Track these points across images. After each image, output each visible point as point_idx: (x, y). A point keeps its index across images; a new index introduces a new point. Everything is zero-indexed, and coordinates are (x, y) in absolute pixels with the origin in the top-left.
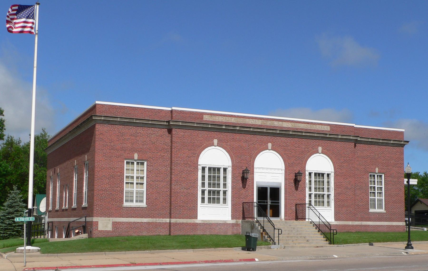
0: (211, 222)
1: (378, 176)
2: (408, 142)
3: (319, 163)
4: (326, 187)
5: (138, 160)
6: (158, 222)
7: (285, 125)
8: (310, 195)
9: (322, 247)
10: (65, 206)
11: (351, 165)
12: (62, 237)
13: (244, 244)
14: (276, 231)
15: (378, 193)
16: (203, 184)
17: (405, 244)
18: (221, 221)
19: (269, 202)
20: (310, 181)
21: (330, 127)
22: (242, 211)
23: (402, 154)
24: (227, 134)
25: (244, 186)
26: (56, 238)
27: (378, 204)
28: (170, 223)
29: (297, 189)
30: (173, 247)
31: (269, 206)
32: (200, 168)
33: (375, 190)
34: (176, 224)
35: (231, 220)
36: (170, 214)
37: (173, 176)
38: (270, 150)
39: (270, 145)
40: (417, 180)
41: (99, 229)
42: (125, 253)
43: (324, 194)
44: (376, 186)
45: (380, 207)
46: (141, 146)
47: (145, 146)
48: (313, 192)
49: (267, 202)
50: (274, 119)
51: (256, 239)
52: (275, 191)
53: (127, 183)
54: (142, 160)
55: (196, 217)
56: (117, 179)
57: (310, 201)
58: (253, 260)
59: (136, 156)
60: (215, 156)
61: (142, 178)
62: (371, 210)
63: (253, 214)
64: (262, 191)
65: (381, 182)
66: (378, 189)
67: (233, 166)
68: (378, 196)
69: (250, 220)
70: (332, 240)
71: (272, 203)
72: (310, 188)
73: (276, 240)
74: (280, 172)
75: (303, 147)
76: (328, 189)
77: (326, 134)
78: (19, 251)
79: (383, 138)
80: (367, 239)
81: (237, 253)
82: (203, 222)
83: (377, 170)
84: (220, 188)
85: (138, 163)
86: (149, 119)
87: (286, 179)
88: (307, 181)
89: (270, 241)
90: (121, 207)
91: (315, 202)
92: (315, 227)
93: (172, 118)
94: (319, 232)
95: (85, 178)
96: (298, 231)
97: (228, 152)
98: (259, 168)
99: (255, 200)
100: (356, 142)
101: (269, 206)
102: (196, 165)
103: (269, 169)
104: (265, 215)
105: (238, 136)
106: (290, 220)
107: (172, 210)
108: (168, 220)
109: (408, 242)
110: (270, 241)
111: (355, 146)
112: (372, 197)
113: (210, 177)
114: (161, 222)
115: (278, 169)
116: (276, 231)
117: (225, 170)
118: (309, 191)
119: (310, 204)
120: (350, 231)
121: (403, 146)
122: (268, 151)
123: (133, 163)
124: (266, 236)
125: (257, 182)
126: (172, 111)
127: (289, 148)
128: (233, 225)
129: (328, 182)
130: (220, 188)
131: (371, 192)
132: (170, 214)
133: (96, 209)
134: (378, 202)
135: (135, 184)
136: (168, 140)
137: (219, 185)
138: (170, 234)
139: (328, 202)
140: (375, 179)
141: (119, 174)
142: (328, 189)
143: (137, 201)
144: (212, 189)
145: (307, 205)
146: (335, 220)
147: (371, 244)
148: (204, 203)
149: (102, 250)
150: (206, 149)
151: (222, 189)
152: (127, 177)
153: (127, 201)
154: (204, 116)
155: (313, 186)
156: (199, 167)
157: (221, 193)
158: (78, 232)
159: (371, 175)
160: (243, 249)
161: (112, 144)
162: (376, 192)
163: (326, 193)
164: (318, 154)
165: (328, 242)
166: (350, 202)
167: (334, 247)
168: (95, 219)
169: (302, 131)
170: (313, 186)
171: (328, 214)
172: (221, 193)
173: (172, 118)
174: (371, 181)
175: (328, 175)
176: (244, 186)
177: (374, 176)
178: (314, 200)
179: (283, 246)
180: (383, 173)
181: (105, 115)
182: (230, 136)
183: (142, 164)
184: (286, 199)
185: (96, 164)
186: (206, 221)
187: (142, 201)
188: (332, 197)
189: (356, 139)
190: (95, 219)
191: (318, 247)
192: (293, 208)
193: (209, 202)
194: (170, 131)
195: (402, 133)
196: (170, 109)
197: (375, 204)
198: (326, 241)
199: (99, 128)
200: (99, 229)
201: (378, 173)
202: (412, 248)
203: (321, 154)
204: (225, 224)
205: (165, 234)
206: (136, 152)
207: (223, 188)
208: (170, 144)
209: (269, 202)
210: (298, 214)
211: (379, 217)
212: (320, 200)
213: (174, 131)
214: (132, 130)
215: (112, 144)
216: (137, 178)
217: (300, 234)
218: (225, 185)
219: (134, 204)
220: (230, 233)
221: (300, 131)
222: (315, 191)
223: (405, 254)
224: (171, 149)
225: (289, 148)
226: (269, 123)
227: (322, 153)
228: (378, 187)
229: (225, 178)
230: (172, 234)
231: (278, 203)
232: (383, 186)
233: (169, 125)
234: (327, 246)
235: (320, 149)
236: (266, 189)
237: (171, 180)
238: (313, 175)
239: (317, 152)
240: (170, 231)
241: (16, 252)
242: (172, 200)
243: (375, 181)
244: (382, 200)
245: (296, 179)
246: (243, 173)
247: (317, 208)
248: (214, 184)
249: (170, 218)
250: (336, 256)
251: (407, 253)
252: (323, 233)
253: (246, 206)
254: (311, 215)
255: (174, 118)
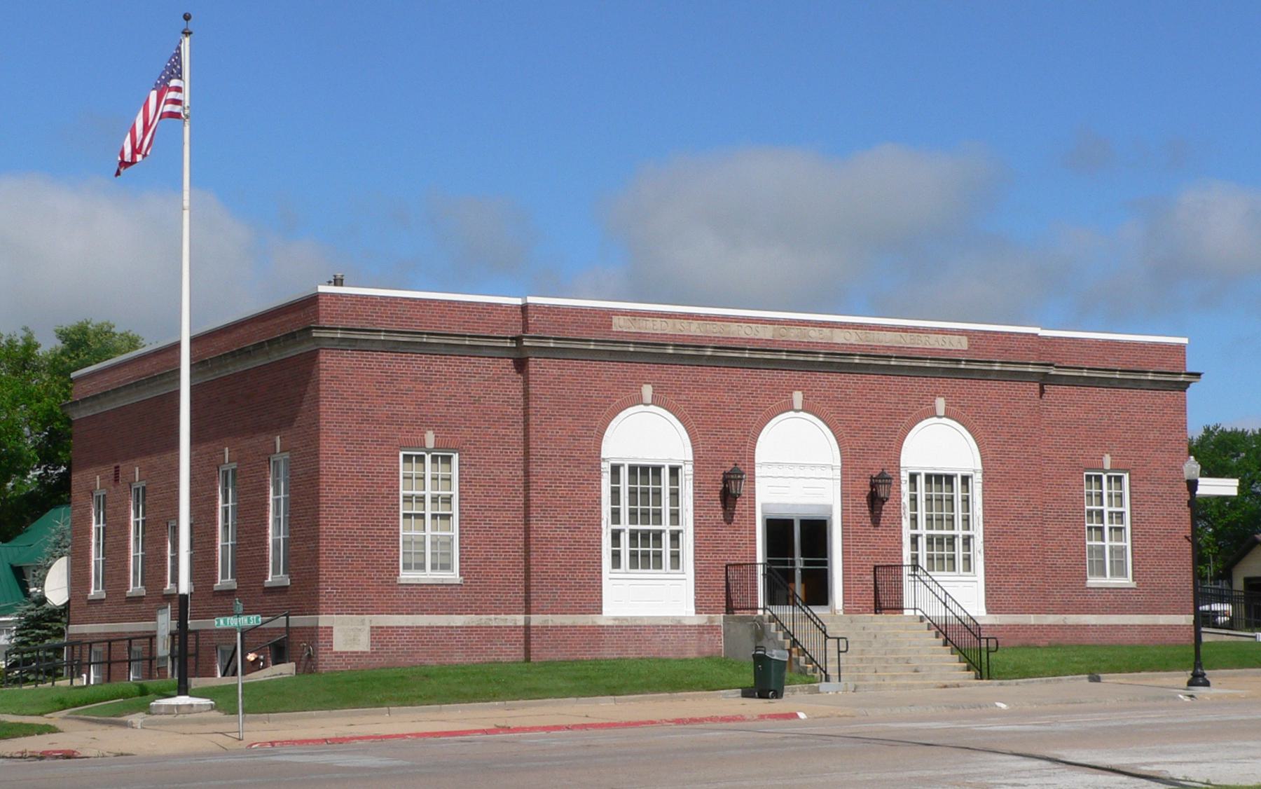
0: (638, 623)
1: (1109, 478)
2: (1198, 375)
3: (939, 445)
4: (959, 514)
5: (436, 448)
6: (494, 624)
7: (840, 337)
8: (914, 540)
9: (958, 686)
10: (175, 580)
11: (1030, 449)
12: (213, 675)
13: (749, 680)
14: (831, 644)
15: (1111, 529)
16: (616, 514)
17: (1186, 676)
18: (666, 618)
19: (799, 562)
20: (914, 499)
21: (969, 338)
22: (722, 588)
23: (1183, 410)
24: (678, 369)
25: (729, 518)
26: (219, 675)
27: (1111, 562)
28: (527, 628)
29: (876, 521)
30: (560, 690)
31: (798, 573)
32: (606, 467)
33: (1102, 522)
34: (545, 629)
35: (693, 614)
36: (527, 600)
37: (532, 494)
38: (797, 411)
39: (798, 397)
40: (1236, 482)
41: (335, 649)
42: (440, 710)
43: (954, 537)
44: (1106, 509)
45: (1119, 570)
46: (443, 411)
47: (453, 411)
48: (923, 530)
49: (793, 563)
50: (809, 321)
51: (782, 665)
52: (816, 531)
53: (406, 516)
54: (447, 449)
55: (598, 610)
56: (381, 506)
57: (915, 558)
58: (794, 716)
59: (430, 439)
60: (645, 434)
61: (448, 500)
62: (1093, 581)
63: (755, 598)
64: (778, 530)
65: (1120, 496)
66: (1111, 517)
67: (698, 461)
68: (1111, 540)
69: (748, 613)
70: (985, 666)
71: (806, 563)
72: (914, 519)
73: (832, 668)
74: (828, 473)
75: (893, 400)
76: (966, 520)
77: (959, 361)
78: (163, 710)
79: (1124, 368)
80: (1082, 663)
81: (729, 702)
82: (617, 623)
83: (1107, 461)
84: (660, 524)
85: (434, 459)
86: (462, 331)
87: (844, 495)
88: (906, 500)
89: (814, 670)
90: (393, 585)
91: (930, 558)
92: (933, 632)
93: (526, 326)
94: (945, 644)
95: (271, 502)
96: (887, 643)
97: (682, 420)
98: (770, 464)
99: (760, 558)
100: (1045, 381)
101: (798, 573)
102: (596, 459)
103: (798, 464)
104: (789, 600)
105: (707, 375)
106: (858, 612)
107: (533, 589)
108: (520, 619)
109: (1195, 669)
110: (814, 670)
111: (1042, 392)
112: (1094, 543)
113: (633, 492)
114: (502, 624)
115: (824, 466)
116: (831, 644)
117: (674, 471)
118: (912, 525)
119: (915, 567)
120: (1033, 642)
121: (1183, 386)
122: (792, 414)
123: (421, 459)
124: (802, 659)
125: (763, 505)
126: (524, 308)
127: (852, 404)
128: (701, 629)
129: (966, 500)
130: (660, 524)
131: (1090, 528)
132: (527, 600)
133: (326, 591)
134: (1111, 556)
135: (432, 522)
136: (516, 391)
137: (658, 515)
138: (528, 660)
139: (967, 559)
140: (1101, 488)
141: (385, 490)
142: (966, 520)
143: (434, 567)
144: (639, 527)
145: (907, 571)
146: (988, 612)
147: (1095, 679)
148: (619, 567)
149: (379, 704)
150: (622, 415)
151: (666, 526)
152: (408, 499)
153: (407, 567)
154: (615, 319)
155: (922, 513)
156: (604, 465)
157: (666, 539)
158: (257, 659)
159: (1089, 477)
160: (747, 693)
161: (365, 406)
162: (1107, 525)
163: (959, 532)
164: (935, 420)
165: (972, 674)
166: (1031, 556)
167: (989, 687)
168: (324, 620)
169: (889, 353)
170: (922, 513)
171: (967, 594)
172: (666, 539)
173: (526, 326)
174: (1090, 495)
175: (965, 480)
176: (729, 518)
177: (1099, 479)
178: (925, 552)
179: (851, 685)
180: (1125, 471)
181: (344, 324)
182: (686, 373)
183: (447, 460)
184: (845, 552)
185: (323, 464)
186: (625, 619)
187: (447, 567)
188: (978, 544)
189: (1047, 371)
190: (324, 620)
191: (946, 687)
192: (868, 577)
193: (634, 565)
194: (521, 365)
195: (1180, 348)
196: (519, 301)
197: (1104, 562)
198: (968, 669)
199: (329, 362)
200: (335, 649)
201: (1112, 470)
202: (1207, 684)
203: (945, 420)
204: (677, 628)
205: (512, 658)
206: (429, 427)
207: (671, 524)
208: (521, 402)
209: (799, 562)
210: (884, 598)
211: (1116, 601)
212: (943, 552)
213: (534, 365)
214: (418, 364)
215: (365, 406)
216: (434, 500)
217: (893, 652)
218: (675, 515)
219: (429, 576)
220: (692, 654)
221: (881, 353)
222: (930, 527)
223: (1187, 699)
224: (526, 415)
225: (852, 404)
226: (793, 334)
227: (804, 410)
228: (1111, 513)
229: (675, 494)
230: (533, 659)
231: (825, 563)
232: (1127, 509)
233: (521, 345)
234: (970, 685)
235: (940, 404)
236: (788, 523)
237: (527, 506)
238: (921, 481)
239: (933, 414)
240: (528, 651)
241: (149, 713)
242: (533, 562)
243: (1101, 495)
244: (1123, 549)
245: (874, 495)
246: (725, 481)
247: (936, 575)
248: (645, 514)
249: (528, 611)
250: (1003, 706)
251: (1191, 696)
252: (957, 649)
253: (734, 575)
254: (919, 598)
255: (531, 327)
